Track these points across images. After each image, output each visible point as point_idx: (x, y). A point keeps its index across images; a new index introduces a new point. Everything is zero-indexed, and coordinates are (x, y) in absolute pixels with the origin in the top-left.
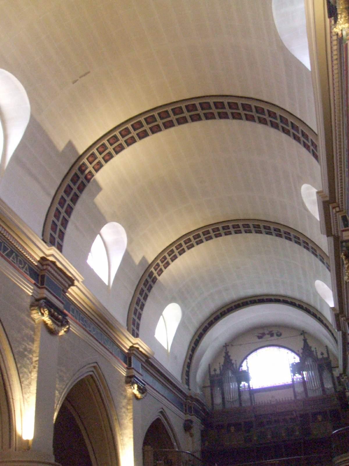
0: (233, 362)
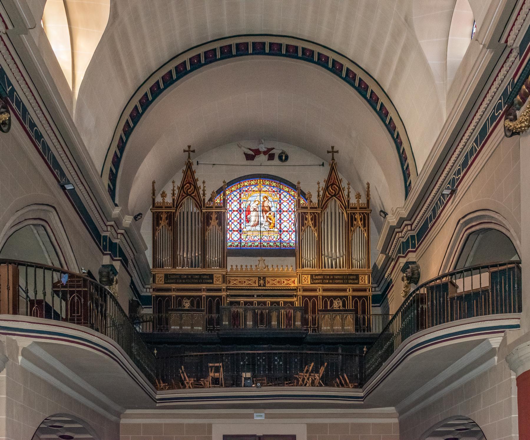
0: (199, 184)
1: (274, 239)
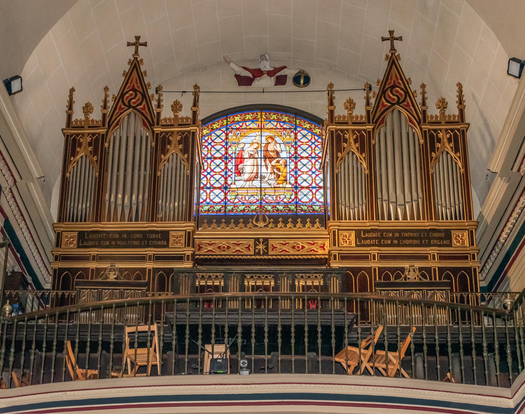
1: (285, 200)
